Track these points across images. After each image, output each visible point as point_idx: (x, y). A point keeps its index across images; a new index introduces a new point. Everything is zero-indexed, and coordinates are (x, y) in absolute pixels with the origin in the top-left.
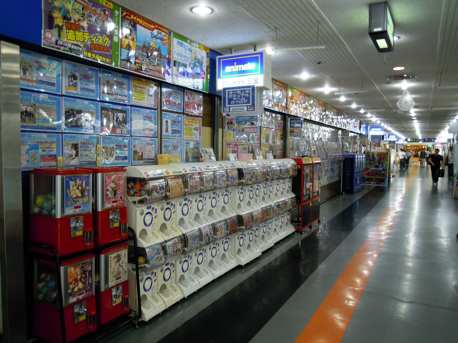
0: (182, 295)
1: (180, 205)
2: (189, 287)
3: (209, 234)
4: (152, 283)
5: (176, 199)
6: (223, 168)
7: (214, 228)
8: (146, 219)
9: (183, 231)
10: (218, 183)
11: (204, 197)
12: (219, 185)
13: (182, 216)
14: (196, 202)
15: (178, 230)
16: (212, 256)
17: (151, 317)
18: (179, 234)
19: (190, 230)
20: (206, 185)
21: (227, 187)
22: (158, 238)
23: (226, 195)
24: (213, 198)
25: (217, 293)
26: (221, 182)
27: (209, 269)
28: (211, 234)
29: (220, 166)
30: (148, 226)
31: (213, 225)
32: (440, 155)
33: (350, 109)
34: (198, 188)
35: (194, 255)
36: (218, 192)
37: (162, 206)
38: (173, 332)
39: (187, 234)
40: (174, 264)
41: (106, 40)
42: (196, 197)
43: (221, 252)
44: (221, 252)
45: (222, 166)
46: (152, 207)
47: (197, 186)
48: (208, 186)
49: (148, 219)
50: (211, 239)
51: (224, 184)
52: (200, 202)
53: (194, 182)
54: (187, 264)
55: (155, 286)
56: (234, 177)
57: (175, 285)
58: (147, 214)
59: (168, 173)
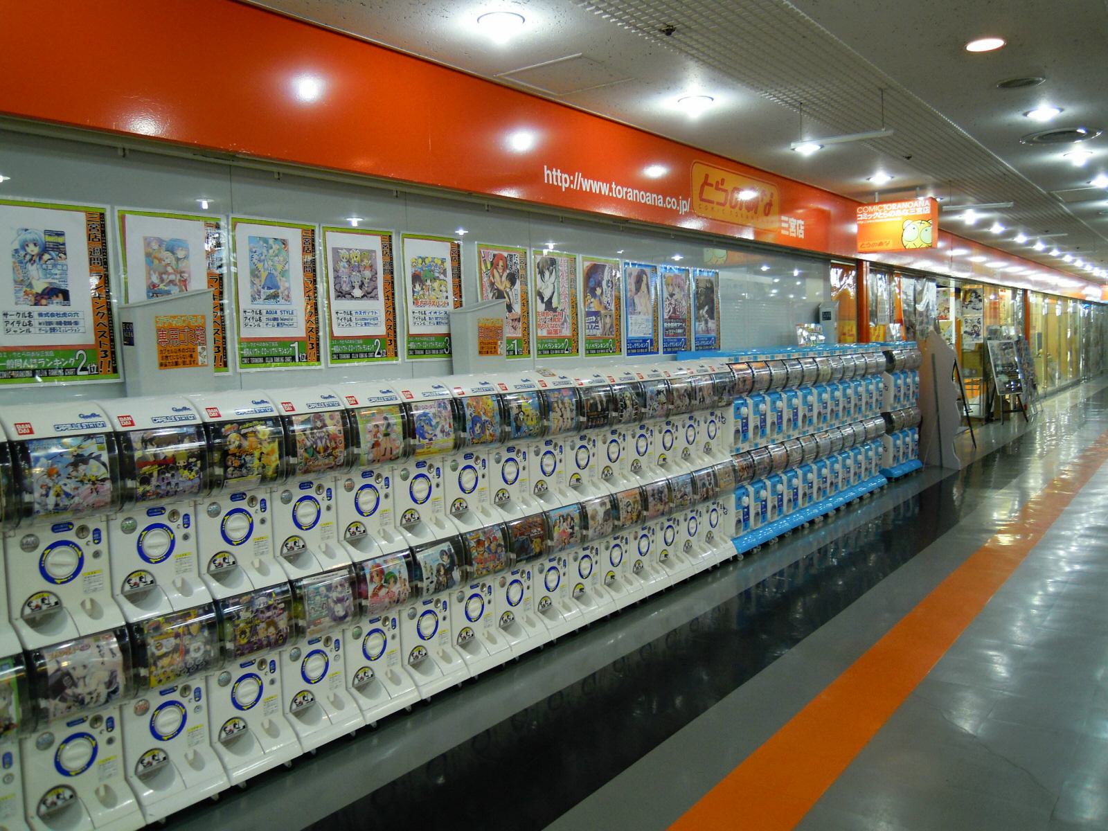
0: (416, 694)
1: (572, 449)
2: (523, 636)
3: (707, 483)
4: (437, 622)
5: (529, 441)
6: (706, 371)
7: (614, 504)
8: (640, 444)
9: (215, 591)
10: (648, 407)
11: (673, 425)
12: (651, 412)
13: (608, 463)
14: (660, 433)
15: (684, 466)
16: (641, 553)
17: (265, 770)
18: (454, 532)
19: (476, 525)
20: (678, 402)
21: (667, 416)
22: (599, 489)
23: (642, 436)
24: (666, 432)
25: (622, 642)
26: (655, 405)
27: (457, 651)
28: (710, 484)
29: (700, 368)
30: (307, 529)
31: (357, 566)
32: (964, 341)
33: (988, 236)
34: (337, 452)
35: (571, 557)
36: (648, 423)
37: (405, 469)
38: (400, 778)
39: (552, 514)
40: (394, 619)
41: (566, 179)
42: (538, 444)
43: (683, 536)
44: (705, 527)
45: (565, 380)
46: (517, 448)
47: (334, 449)
48: (681, 404)
49: (468, 478)
50: (711, 493)
51: (662, 408)
52: (642, 438)
53: (321, 438)
54: (647, 543)
55: (276, 696)
56: (484, 418)
57: (452, 649)
58: (464, 468)
59: (409, 396)
